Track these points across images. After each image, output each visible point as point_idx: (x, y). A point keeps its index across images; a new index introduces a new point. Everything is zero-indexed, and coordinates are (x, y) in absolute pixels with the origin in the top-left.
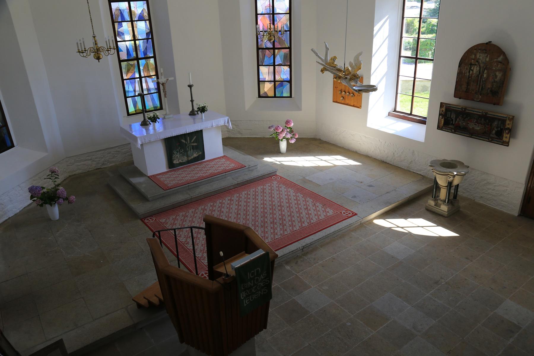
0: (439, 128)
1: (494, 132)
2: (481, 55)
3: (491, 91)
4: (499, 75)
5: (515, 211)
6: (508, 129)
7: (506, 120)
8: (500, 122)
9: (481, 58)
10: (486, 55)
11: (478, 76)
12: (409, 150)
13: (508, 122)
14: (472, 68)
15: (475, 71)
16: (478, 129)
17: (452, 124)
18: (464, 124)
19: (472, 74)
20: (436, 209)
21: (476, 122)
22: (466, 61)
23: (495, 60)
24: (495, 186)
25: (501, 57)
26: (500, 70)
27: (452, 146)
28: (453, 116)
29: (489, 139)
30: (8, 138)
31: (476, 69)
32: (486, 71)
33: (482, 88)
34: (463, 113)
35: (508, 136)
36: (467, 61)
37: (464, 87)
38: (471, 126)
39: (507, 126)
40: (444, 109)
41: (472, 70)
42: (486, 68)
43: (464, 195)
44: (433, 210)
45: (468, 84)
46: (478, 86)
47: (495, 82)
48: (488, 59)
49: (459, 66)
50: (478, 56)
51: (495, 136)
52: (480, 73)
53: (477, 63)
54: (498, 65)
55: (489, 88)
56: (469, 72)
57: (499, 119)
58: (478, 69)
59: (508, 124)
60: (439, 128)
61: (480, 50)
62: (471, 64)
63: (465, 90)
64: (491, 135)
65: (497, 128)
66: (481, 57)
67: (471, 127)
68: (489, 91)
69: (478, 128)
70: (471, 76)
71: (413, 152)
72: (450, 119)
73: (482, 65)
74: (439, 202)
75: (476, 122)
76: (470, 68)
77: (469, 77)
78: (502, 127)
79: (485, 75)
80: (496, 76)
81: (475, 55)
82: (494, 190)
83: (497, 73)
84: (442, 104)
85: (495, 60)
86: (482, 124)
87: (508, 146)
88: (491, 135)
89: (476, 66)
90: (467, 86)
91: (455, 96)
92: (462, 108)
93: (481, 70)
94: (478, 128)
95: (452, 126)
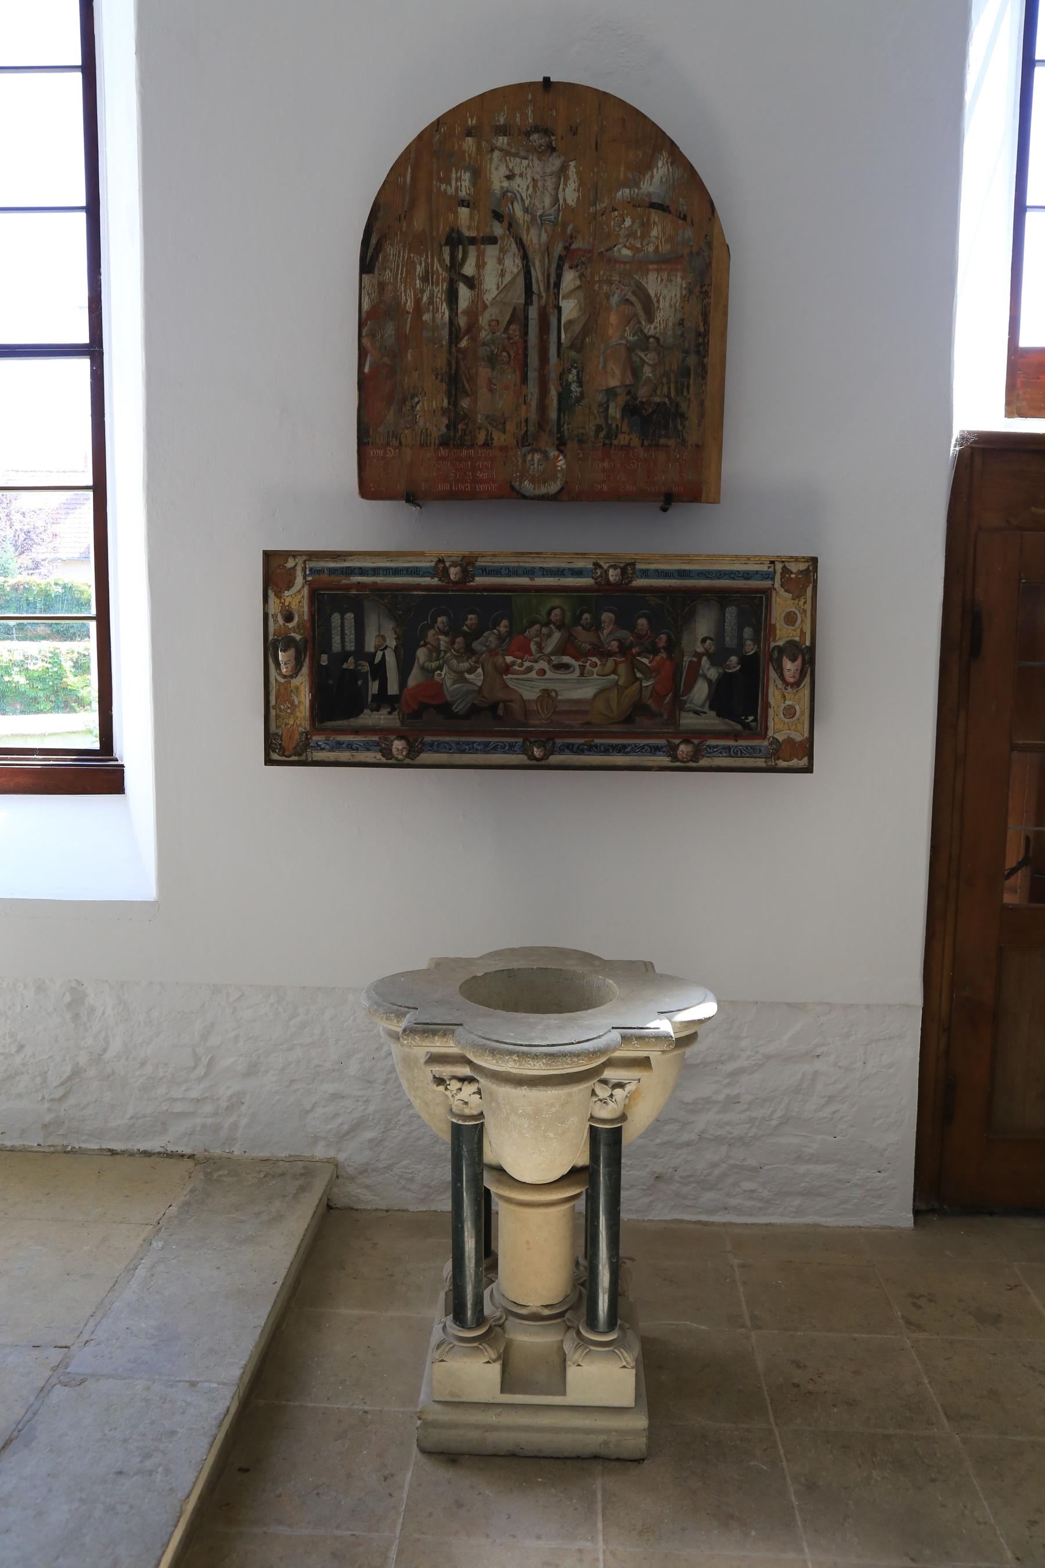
0: (279, 750)
1: (701, 691)
2: (518, 165)
3: (631, 410)
4: (667, 292)
5: (889, 1196)
6: (793, 649)
7: (767, 592)
8: (731, 612)
9: (521, 185)
10: (555, 163)
11: (519, 318)
12: (41, 988)
13: (782, 603)
14: (469, 269)
15: (490, 284)
16: (587, 692)
17: (383, 700)
18: (477, 678)
19: (473, 314)
20: (530, 1423)
21: (561, 650)
22: (416, 218)
23: (623, 194)
24: (741, 1071)
25: (661, 170)
26: (667, 262)
27: (408, 860)
28: (381, 636)
29: (672, 751)
30: (727, 628)
31: (495, 273)
32: (569, 279)
33: (564, 395)
34: (459, 604)
35: (799, 700)
36: (419, 222)
37: (429, 408)
38: (529, 683)
39: (784, 634)
40: (297, 597)
41: (471, 283)
42: (567, 257)
43: (662, 1213)
44: (505, 1440)
45: (455, 382)
46: (532, 389)
47: (644, 341)
48: (570, 194)
49: (367, 265)
50: (497, 180)
51: (710, 720)
52: (535, 298)
53: (498, 230)
54: (646, 226)
55: (611, 393)
56: (452, 297)
57: (722, 598)
58: (513, 265)
59: (790, 619)
60: (279, 750)
61: (503, 130)
62: (455, 240)
63: (439, 427)
64: (688, 721)
65: (717, 658)
66: (521, 179)
67: (530, 693)
68: (581, 431)
69: (581, 687)
70: (472, 327)
71: (77, 999)
72: (362, 670)
73: (535, 238)
74: (528, 1339)
75: (561, 650)
76: (455, 266)
77: (455, 335)
78: (750, 648)
79: (570, 308)
80: (649, 307)
81: (477, 174)
82: (733, 1101)
83: (653, 284)
84: (276, 569)
85: (623, 194)
86: (604, 654)
87: (809, 769)
88: (688, 721)
89: (491, 252)
90: (454, 402)
91: (368, 489)
92: (440, 568)
93: (537, 273)
94: (581, 687)
95: (381, 718)
